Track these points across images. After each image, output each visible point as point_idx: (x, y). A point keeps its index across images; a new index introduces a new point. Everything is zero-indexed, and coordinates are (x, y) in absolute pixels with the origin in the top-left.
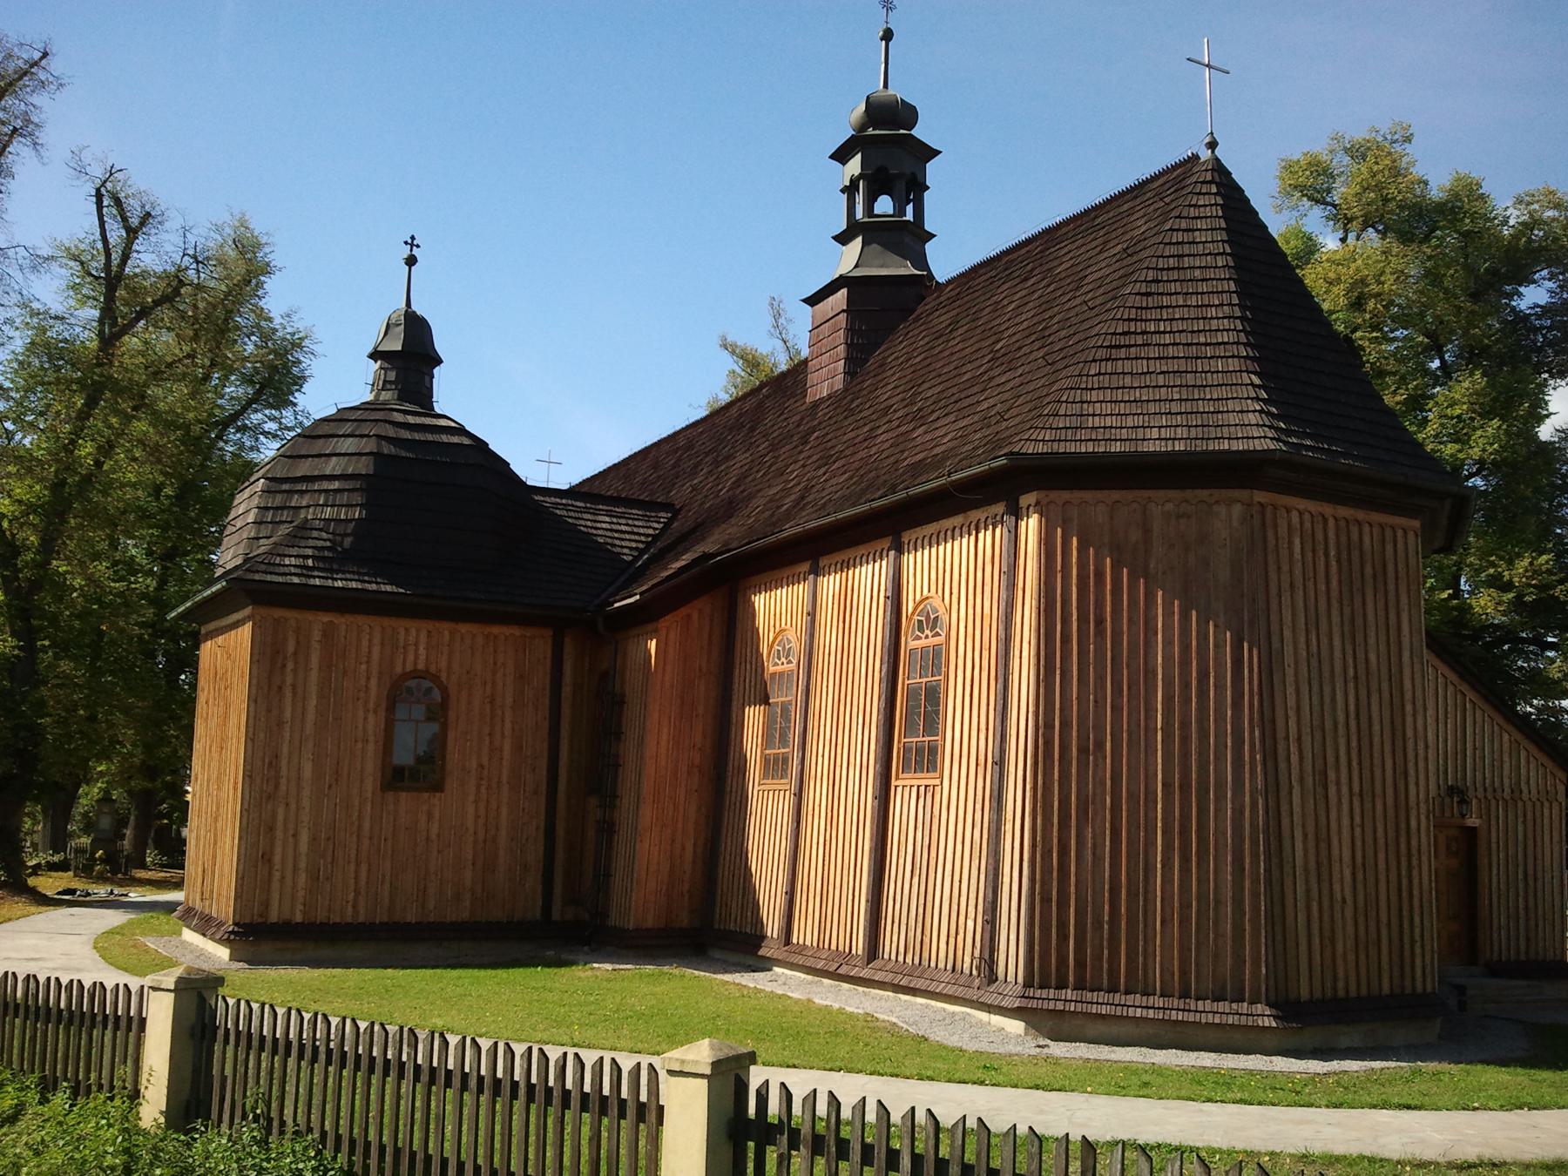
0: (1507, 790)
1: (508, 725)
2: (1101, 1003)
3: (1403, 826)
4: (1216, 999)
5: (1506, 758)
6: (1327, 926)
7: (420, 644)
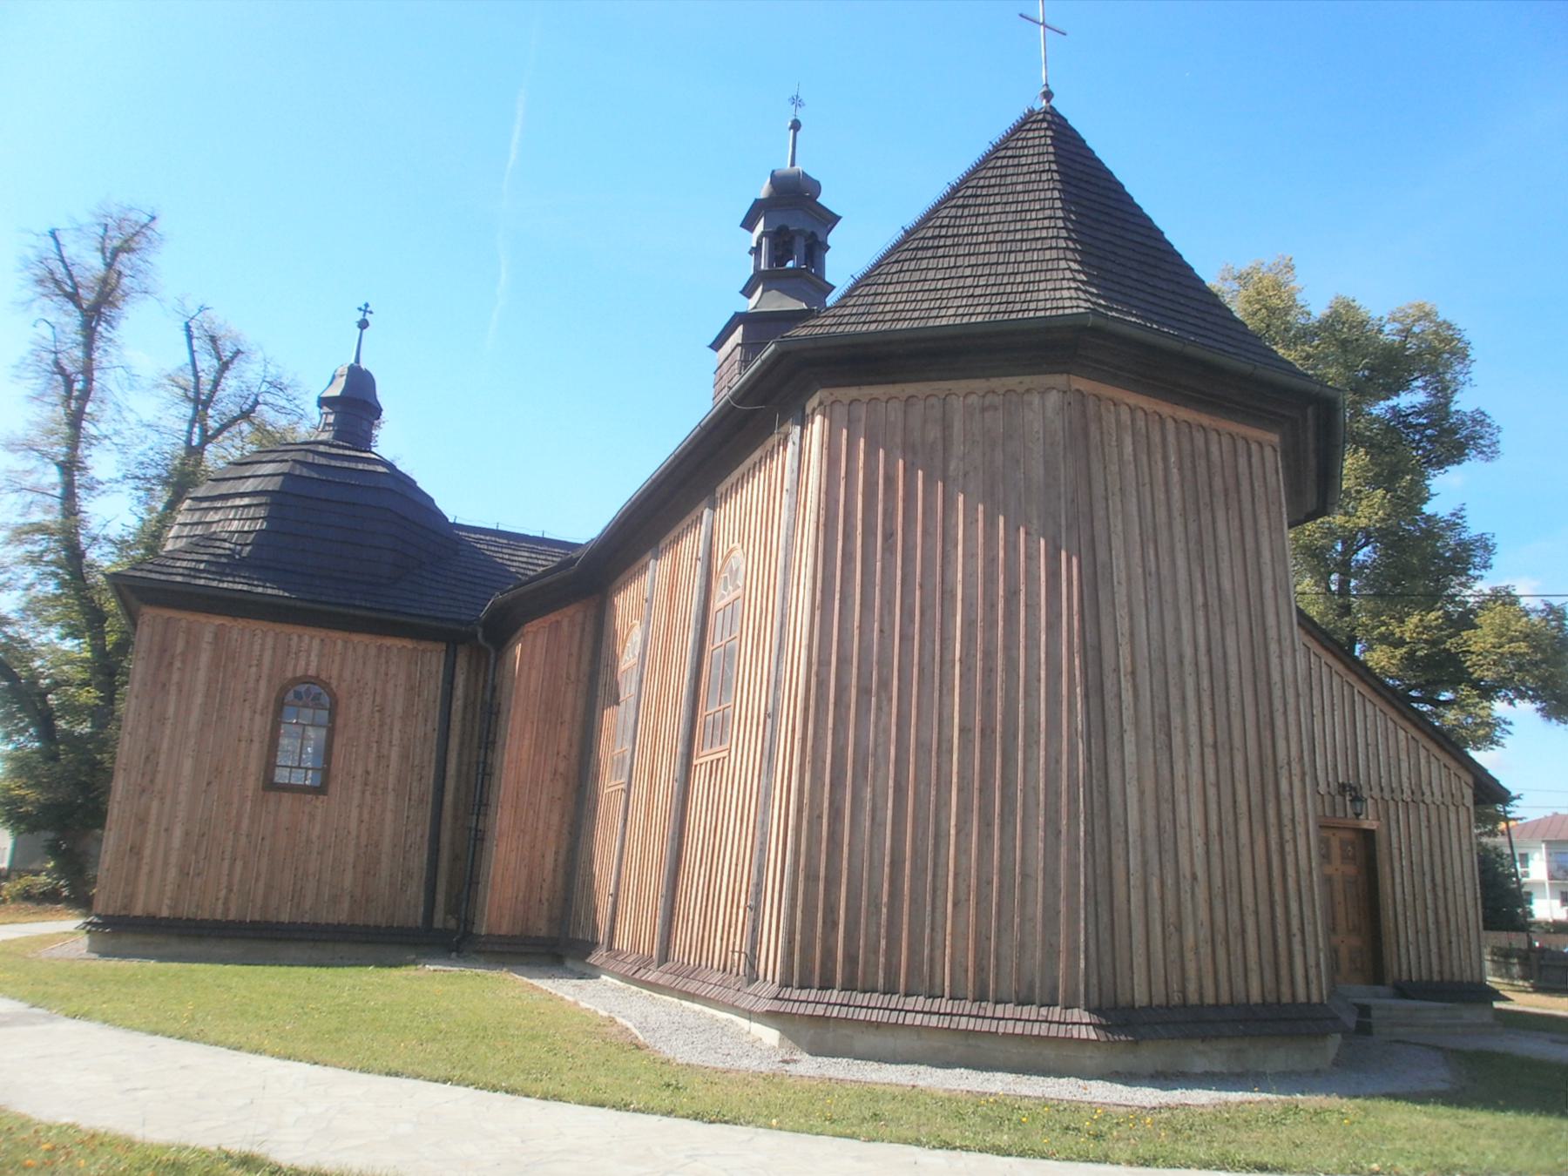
0: (1407, 792)
1: (396, 733)
2: (870, 1007)
3: (1270, 788)
4: (1021, 1003)
5: (1403, 756)
7: (310, 650)
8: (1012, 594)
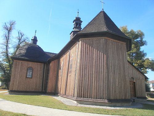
2: (86, 99)
6: (115, 89)
7: (31, 64)
8: (99, 59)
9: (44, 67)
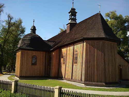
2: (91, 83)
7: (35, 53)
8: (99, 56)
9: (46, 55)
